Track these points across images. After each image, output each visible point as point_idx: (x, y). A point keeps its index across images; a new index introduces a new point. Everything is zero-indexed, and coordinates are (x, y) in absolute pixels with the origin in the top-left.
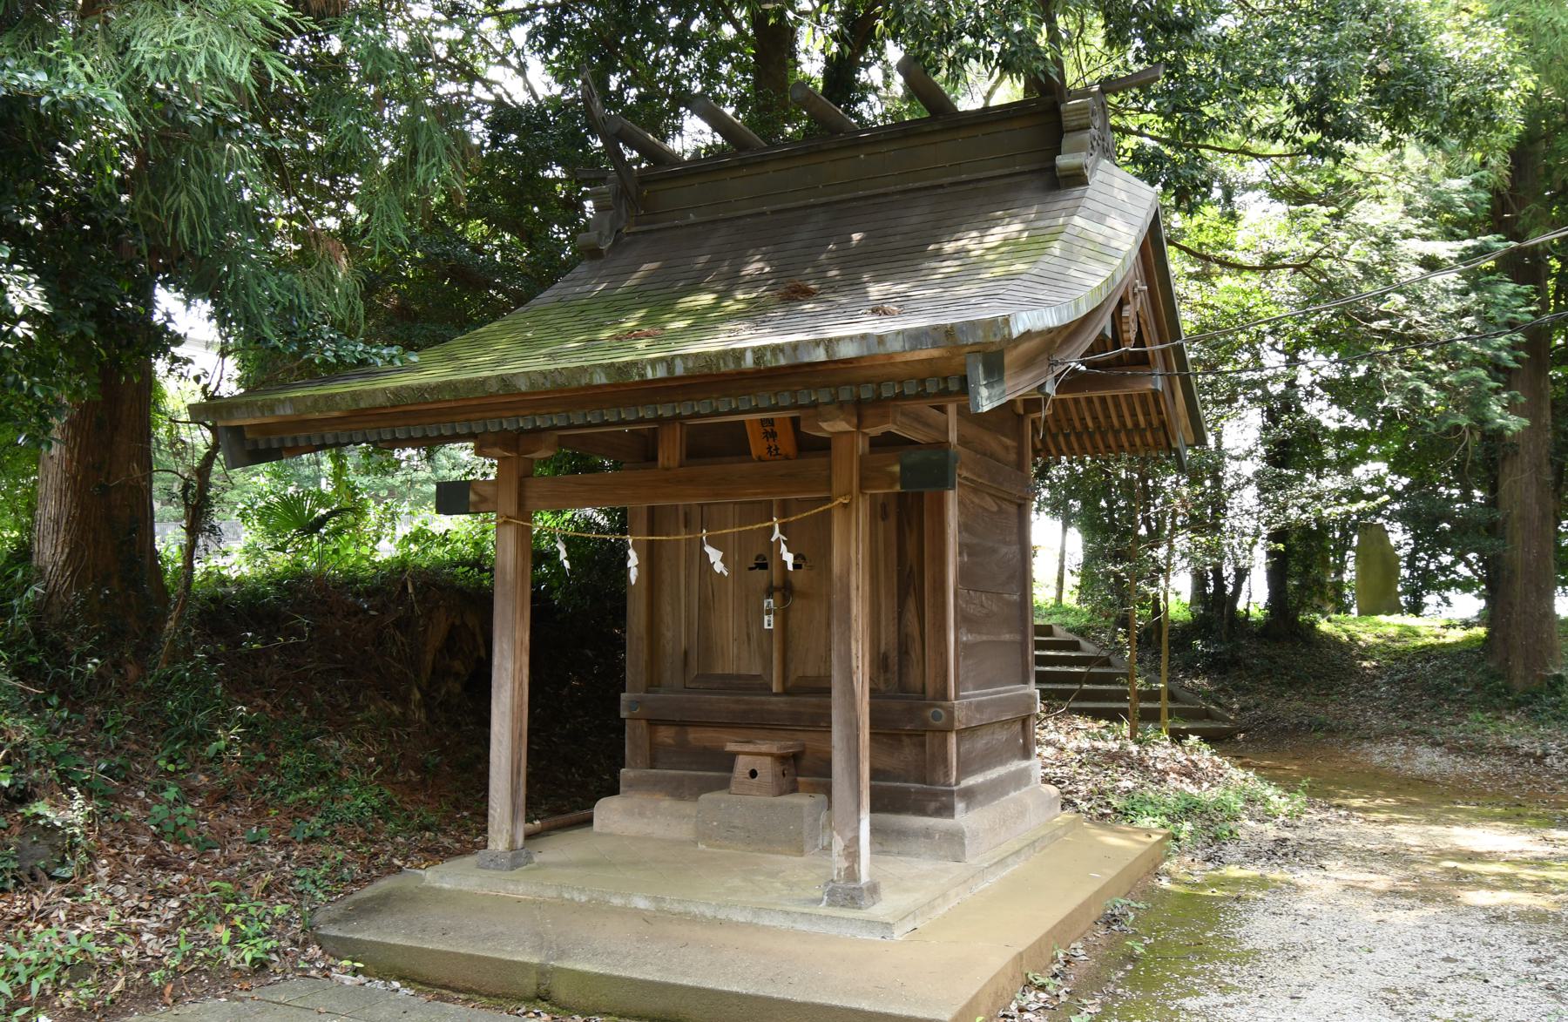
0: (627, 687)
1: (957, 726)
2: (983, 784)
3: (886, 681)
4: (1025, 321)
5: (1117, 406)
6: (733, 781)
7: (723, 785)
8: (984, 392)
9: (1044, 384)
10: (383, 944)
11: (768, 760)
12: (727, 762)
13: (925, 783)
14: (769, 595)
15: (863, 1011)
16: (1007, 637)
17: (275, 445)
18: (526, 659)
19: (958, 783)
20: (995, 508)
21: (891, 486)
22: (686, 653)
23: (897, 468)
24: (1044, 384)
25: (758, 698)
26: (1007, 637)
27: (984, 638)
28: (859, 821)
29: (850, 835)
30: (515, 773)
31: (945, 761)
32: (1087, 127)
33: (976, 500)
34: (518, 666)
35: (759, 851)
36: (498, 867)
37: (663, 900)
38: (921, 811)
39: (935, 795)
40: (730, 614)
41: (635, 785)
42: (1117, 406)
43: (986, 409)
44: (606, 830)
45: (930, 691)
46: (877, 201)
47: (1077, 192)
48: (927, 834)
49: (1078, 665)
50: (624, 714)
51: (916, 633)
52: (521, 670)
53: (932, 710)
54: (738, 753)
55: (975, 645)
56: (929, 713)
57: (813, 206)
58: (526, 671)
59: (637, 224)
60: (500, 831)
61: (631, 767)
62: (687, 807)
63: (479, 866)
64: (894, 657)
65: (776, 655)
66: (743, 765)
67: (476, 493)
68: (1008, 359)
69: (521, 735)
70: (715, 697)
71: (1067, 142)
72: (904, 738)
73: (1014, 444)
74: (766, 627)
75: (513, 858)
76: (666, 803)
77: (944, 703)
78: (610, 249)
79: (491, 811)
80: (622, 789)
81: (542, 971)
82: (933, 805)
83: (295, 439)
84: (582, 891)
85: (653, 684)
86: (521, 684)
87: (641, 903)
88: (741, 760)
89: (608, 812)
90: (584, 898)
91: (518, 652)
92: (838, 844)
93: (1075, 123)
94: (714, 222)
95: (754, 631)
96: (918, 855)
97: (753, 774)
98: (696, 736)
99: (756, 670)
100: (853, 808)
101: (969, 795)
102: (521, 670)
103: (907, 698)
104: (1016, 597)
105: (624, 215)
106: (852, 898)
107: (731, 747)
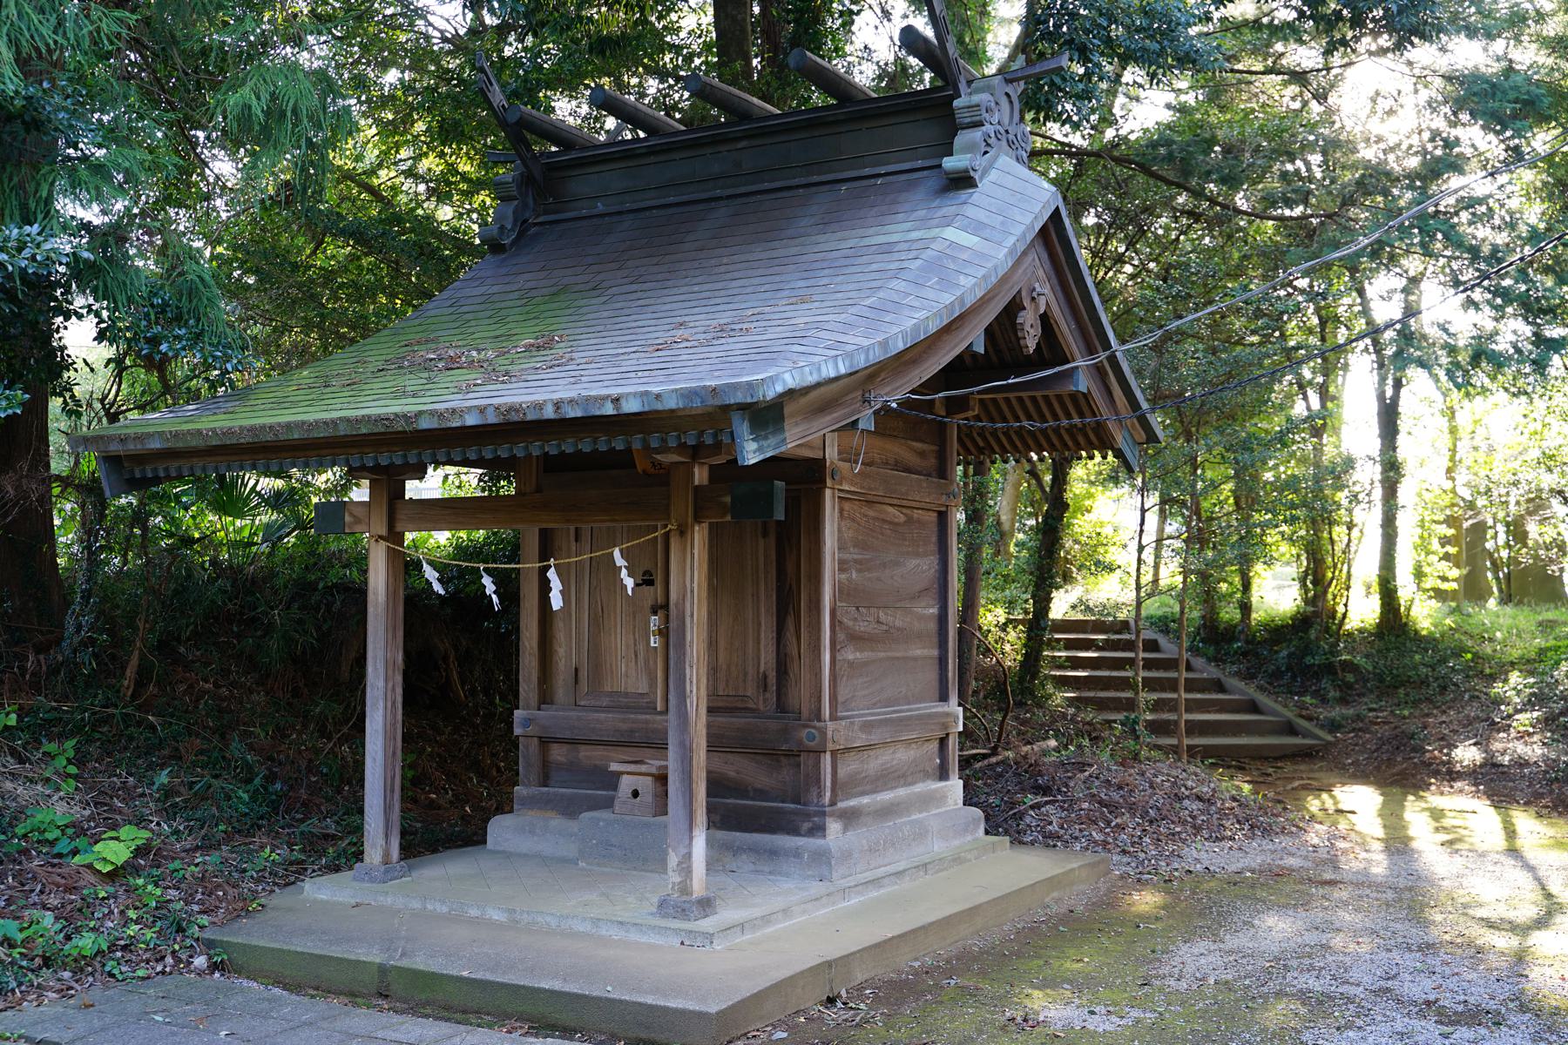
0: (521, 704)
1: (830, 746)
2: (868, 805)
3: (765, 700)
4: (785, 377)
5: (1050, 405)
6: (616, 802)
7: (608, 804)
8: (752, 446)
9: (857, 420)
10: (250, 946)
11: (650, 778)
12: (612, 780)
13: (799, 803)
14: (655, 613)
15: (646, 1005)
16: (926, 652)
17: (150, 475)
18: (399, 678)
19: (833, 803)
20: (902, 518)
21: (724, 515)
22: (576, 670)
23: (728, 499)
24: (857, 420)
25: (644, 717)
26: (926, 652)
27: (882, 655)
28: (691, 838)
29: (683, 851)
30: (388, 790)
31: (818, 781)
32: (980, 124)
33: (871, 513)
34: (390, 685)
35: (635, 869)
36: (372, 880)
37: (515, 911)
38: (795, 831)
39: (808, 816)
40: (619, 631)
41: (532, 803)
42: (1050, 405)
43: (752, 462)
44: (499, 848)
45: (805, 713)
46: (780, 195)
47: (963, 194)
48: (797, 853)
49: (1084, 668)
50: (517, 731)
51: (795, 652)
52: (393, 689)
53: (807, 730)
54: (622, 773)
55: (866, 664)
56: (804, 733)
57: (721, 198)
58: (399, 691)
59: (546, 213)
60: (373, 846)
61: (524, 784)
62: (573, 826)
63: (355, 879)
64: (772, 676)
65: (660, 674)
66: (627, 784)
67: (351, 514)
68: (787, 411)
69: (394, 753)
70: (603, 715)
71: (961, 139)
72: (782, 758)
73: (934, 448)
74: (652, 644)
75: (386, 871)
76: (557, 821)
77: (818, 724)
78: (514, 243)
79: (366, 826)
80: (515, 807)
81: (383, 970)
82: (806, 826)
83: (166, 469)
84: (443, 902)
85: (545, 698)
86: (394, 703)
87: (496, 915)
88: (625, 779)
89: (500, 829)
90: (445, 909)
91: (390, 672)
92: (673, 860)
93: (969, 120)
94: (620, 213)
95: (641, 647)
96: (787, 875)
97: (635, 794)
98: (585, 753)
99: (643, 688)
100: (686, 826)
101: (850, 818)
102: (393, 689)
103: (784, 718)
104: (934, 611)
105: (531, 202)
106: (684, 910)
107: (614, 767)
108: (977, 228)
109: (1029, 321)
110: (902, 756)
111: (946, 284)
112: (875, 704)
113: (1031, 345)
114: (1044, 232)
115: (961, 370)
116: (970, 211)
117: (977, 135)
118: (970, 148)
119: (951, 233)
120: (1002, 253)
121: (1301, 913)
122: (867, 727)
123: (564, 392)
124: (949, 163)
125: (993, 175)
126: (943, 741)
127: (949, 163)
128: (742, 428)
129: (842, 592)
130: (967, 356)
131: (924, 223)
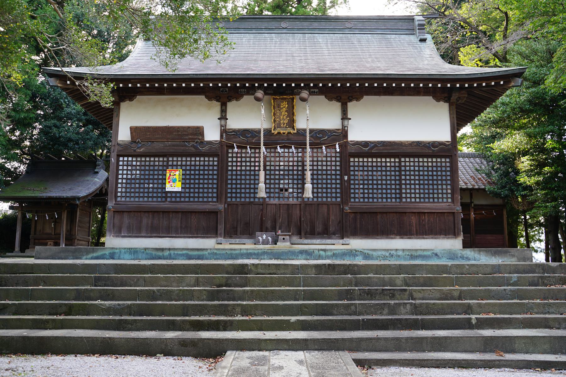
85: (35, 234)
99: (51, 232)
108: (99, 179)
109: (104, 189)
110: (84, 243)
111: (95, 185)
112: (371, 70)
113: (104, 192)
114: (107, 179)
115: (97, 195)
116: (98, 177)
117: (99, 167)
118: (98, 169)
119: (96, 179)
120: (101, 182)
121: (165, 53)
122: (81, 237)
123: (57, 195)
124: (95, 170)
125: (101, 172)
126: (89, 242)
127: (95, 170)
128: (77, 200)
129: (79, 221)
130: (97, 193)
131: (92, 177)
